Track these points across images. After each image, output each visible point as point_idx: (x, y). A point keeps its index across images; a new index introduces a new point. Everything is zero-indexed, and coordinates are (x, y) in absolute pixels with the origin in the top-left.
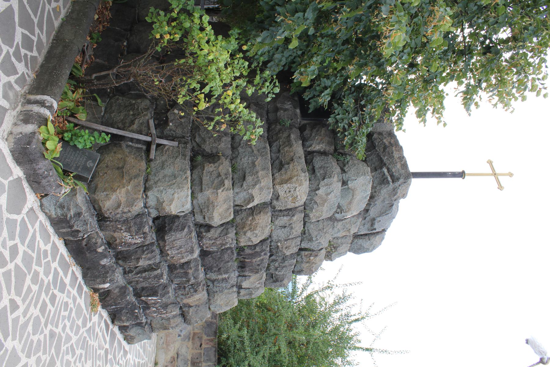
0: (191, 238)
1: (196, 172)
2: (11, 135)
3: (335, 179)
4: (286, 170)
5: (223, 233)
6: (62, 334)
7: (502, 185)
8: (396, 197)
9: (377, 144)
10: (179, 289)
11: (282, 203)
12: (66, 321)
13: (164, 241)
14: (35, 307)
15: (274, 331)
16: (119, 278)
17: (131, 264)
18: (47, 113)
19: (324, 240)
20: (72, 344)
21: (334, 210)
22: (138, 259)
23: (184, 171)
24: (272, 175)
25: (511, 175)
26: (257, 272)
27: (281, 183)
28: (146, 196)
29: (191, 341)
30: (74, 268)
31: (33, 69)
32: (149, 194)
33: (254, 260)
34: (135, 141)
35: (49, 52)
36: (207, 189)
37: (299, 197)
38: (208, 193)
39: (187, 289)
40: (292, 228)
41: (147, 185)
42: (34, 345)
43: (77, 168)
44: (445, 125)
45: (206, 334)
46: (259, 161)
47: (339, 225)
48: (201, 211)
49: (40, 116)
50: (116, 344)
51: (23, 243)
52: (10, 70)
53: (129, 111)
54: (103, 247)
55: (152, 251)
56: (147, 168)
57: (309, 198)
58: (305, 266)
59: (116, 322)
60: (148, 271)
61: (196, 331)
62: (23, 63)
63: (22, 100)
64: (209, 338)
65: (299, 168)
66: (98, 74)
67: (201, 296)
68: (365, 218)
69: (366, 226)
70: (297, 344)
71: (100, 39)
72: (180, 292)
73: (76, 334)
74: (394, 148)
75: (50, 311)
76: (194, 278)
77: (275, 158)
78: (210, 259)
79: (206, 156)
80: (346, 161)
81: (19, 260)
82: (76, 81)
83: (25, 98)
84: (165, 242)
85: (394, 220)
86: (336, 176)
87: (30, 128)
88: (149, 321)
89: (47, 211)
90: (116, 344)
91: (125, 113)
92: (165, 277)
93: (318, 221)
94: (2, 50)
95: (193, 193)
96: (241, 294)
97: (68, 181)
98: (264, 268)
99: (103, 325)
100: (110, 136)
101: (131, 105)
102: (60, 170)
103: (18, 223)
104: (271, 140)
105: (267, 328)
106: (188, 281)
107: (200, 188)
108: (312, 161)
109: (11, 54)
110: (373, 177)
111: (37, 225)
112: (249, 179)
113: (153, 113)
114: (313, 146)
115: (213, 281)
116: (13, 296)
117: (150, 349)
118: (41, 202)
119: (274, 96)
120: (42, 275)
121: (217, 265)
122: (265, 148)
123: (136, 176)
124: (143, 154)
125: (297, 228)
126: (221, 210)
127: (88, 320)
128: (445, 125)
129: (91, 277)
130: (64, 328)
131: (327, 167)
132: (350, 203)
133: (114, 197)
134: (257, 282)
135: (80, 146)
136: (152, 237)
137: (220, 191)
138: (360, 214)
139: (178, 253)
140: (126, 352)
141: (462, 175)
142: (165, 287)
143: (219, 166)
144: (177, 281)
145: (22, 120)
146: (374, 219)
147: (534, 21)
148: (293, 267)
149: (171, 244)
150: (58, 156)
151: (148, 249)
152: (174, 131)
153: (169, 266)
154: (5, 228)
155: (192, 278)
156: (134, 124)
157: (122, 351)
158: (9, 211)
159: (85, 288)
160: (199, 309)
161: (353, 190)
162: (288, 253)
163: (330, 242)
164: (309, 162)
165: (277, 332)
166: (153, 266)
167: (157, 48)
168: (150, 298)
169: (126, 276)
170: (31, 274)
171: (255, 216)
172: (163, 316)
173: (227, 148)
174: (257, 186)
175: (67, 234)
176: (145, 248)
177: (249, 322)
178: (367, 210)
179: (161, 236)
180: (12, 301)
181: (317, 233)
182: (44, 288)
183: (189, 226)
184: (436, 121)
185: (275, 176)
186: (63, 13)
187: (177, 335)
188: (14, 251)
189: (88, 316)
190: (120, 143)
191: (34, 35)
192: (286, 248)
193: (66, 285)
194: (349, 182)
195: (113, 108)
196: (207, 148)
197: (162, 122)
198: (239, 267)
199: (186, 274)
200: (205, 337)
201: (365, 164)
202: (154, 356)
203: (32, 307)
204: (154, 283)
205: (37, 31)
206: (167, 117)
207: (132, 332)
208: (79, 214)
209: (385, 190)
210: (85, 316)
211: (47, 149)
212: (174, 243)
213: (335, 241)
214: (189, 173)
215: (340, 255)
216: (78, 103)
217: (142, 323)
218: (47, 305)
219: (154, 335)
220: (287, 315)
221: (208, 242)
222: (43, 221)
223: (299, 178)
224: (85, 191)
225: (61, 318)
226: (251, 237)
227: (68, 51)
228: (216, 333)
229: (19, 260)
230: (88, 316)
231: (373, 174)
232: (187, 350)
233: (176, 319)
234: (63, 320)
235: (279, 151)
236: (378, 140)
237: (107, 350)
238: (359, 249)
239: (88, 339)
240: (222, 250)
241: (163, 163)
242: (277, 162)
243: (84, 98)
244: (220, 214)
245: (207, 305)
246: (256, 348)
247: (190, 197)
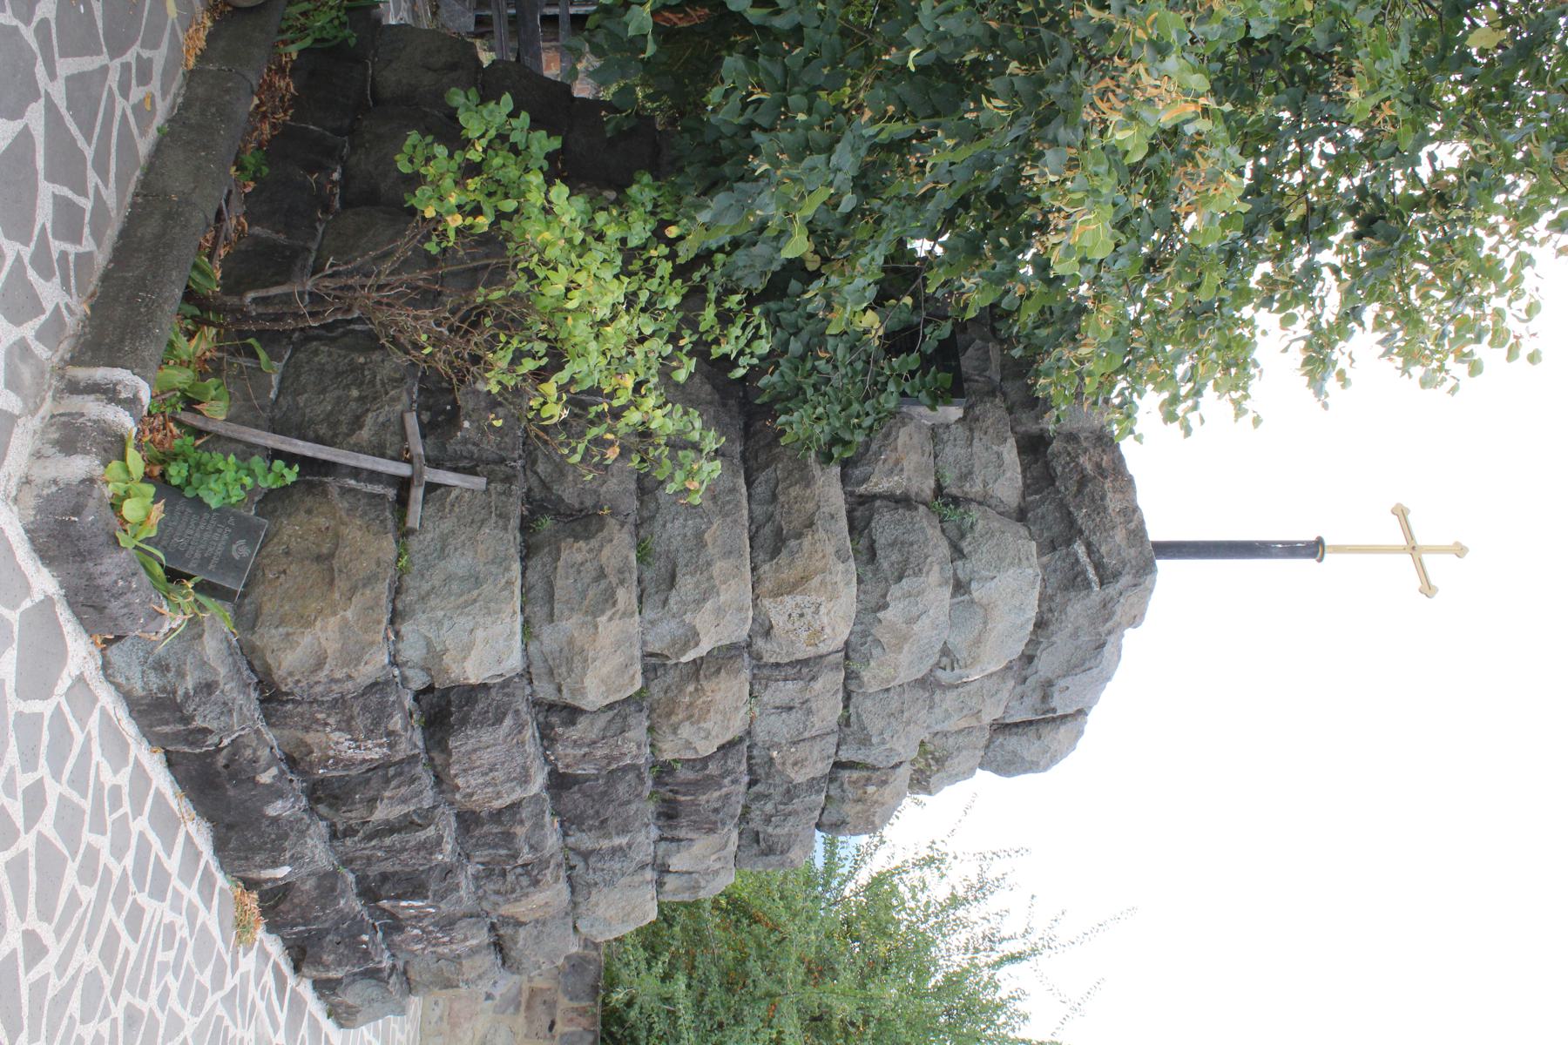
0: (523, 743)
1: (536, 563)
3: (934, 577)
4: (792, 553)
5: (614, 728)
6: (158, 1014)
7: (1433, 582)
8: (1109, 625)
9: (1059, 470)
10: (487, 877)
11: (780, 645)
12: (169, 977)
13: (446, 751)
14: (89, 947)
15: (766, 984)
16: (317, 851)
17: (353, 815)
18: (125, 422)
19: (903, 741)
20: (185, 1039)
22: (372, 802)
23: (501, 562)
24: (753, 569)
25: (1460, 551)
26: (711, 831)
27: (777, 593)
28: (397, 634)
30: (192, 827)
31: (81, 288)
32: (405, 628)
35: (123, 234)
36: (567, 613)
37: (828, 630)
38: (570, 624)
39: (511, 878)
40: (809, 712)
41: (400, 606)
43: (204, 562)
44: (1257, 421)
45: (566, 992)
46: (715, 532)
47: (949, 700)
50: (304, 1030)
52: (21, 304)
53: (348, 387)
54: (274, 771)
55: (413, 780)
56: (400, 555)
57: (859, 628)
58: (850, 810)
59: (305, 970)
60: (399, 831)
61: (539, 983)
62: (57, 280)
63: (54, 383)
64: (575, 1004)
65: (830, 550)
66: (262, 293)
67: (552, 894)
68: (1025, 680)
69: (1028, 701)
70: (835, 1024)
71: (265, 170)
72: (490, 887)
73: (196, 1010)
74: (1108, 484)
75: (127, 952)
76: (531, 847)
78: (577, 796)
80: (968, 521)
81: (46, 824)
82: (199, 306)
83: (63, 377)
84: (450, 755)
86: (936, 568)
87: (79, 466)
88: (400, 965)
89: (121, 680)
90: (304, 1030)
91: (337, 393)
92: (448, 848)
93: (887, 690)
95: (526, 624)
96: (667, 887)
97: (180, 600)
98: (732, 817)
99: (269, 978)
101: (355, 369)
102: (159, 571)
103: (46, 723)
105: (747, 975)
107: (546, 609)
108: (869, 523)
109: (26, 260)
110: (1044, 567)
111: (94, 721)
112: (687, 584)
113: (415, 389)
114: (874, 480)
115: (586, 855)
116: (32, 922)
117: (403, 1039)
118: (104, 657)
119: (755, 361)
120: (105, 857)
121: (597, 812)
122: (733, 490)
123: (370, 580)
124: (388, 513)
125: (825, 711)
126: (605, 670)
127: (49, 230)
128: (1257, 421)
130: (163, 999)
131: (912, 544)
132: (978, 642)
133: (306, 640)
135: (214, 503)
136: (412, 740)
137: (603, 619)
138: (1008, 668)
139: (486, 785)
141: (1314, 549)
142: (448, 871)
143: (602, 546)
144: (481, 855)
145: (56, 443)
146: (1049, 684)
147: (1498, 148)
148: (817, 813)
150: (153, 534)
151: (401, 774)
152: (474, 444)
153: (458, 815)
154: (13, 741)
155: (526, 849)
156: (361, 427)
159: (221, 880)
160: (547, 930)
161: (985, 608)
163: (922, 743)
164: (858, 526)
165: (776, 988)
166: (415, 818)
168: (404, 903)
169: (336, 843)
170: (79, 857)
172: (440, 950)
173: (626, 490)
174: (709, 605)
175: (176, 737)
176: (391, 771)
177: (694, 957)
178: (1028, 659)
180: (30, 937)
182: (112, 890)
183: (517, 712)
184: (1230, 409)
185: (761, 571)
186: (162, 110)
188: (35, 799)
189: (228, 959)
190: (322, 484)
191: (85, 194)
192: (795, 764)
193: (170, 875)
194: (974, 585)
195: (303, 379)
196: (568, 494)
197: (441, 416)
198: (659, 815)
199: (508, 837)
200: (564, 1002)
201: (1023, 532)
204: (416, 862)
205: (93, 178)
206: (454, 402)
207: (349, 997)
208: (208, 687)
209: (1078, 607)
210: (220, 958)
211: (124, 521)
212: (474, 757)
213: (937, 741)
214: (516, 567)
215: (954, 778)
216: (208, 368)
217: (380, 970)
218: (119, 938)
219: (415, 1003)
220: (804, 940)
221: (569, 751)
224: (227, 627)
226: (693, 739)
227: (177, 229)
229: (46, 824)
230: (228, 959)
231: (1045, 559)
234: (161, 977)
236: (1064, 459)
238: (1010, 763)
239: (227, 1021)
240: (612, 772)
241: (444, 541)
242: (767, 530)
244: (602, 679)
245: (570, 920)
247: (518, 637)
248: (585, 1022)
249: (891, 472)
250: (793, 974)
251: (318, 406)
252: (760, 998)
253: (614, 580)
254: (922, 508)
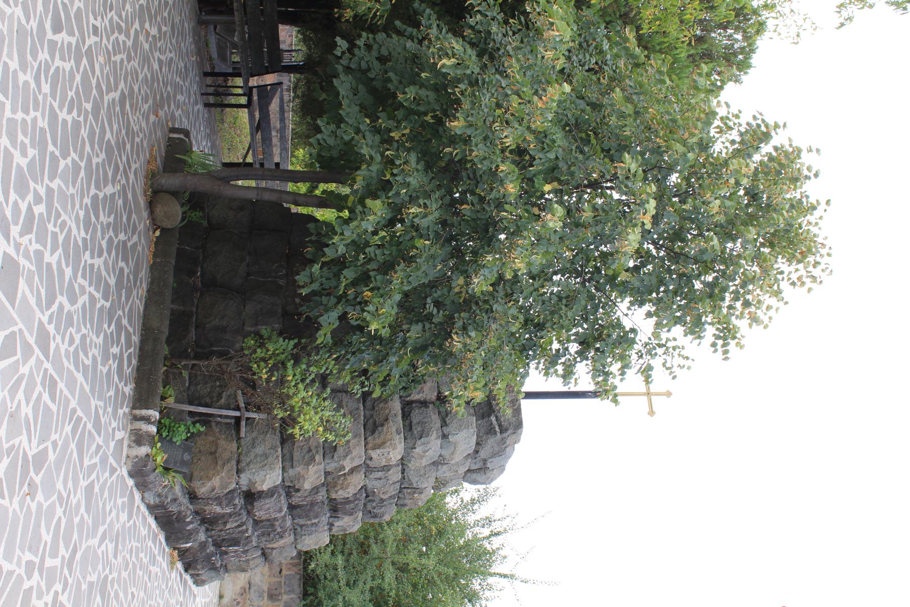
1: (286, 446)
16: (202, 537)
22: (225, 523)
24: (365, 439)
27: (374, 449)
38: (299, 469)
53: (215, 381)
65: (394, 429)
67: (289, 539)
77: (368, 416)
87: (144, 450)
95: (283, 468)
115: (302, 526)
122: (358, 409)
123: (229, 460)
132: (453, 453)
159: (167, 549)
164: (406, 415)
178: (476, 452)
210: (60, 493)
233: (256, 561)
235: (374, 408)
241: (254, 440)
242: (371, 421)
248: (295, 569)
249: (419, 393)
250: (391, 548)
251: (203, 390)
253: (314, 451)
254: (431, 406)
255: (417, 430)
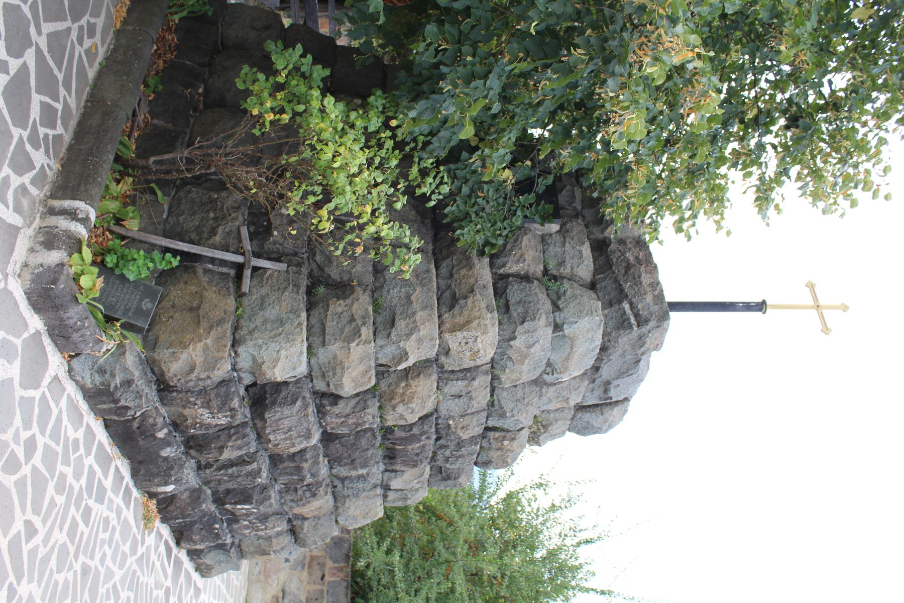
0: (307, 415)
1: (315, 313)
2: (25, 269)
3: (542, 321)
4: (461, 308)
8: (643, 349)
9: (615, 260)
10: (287, 492)
11: (454, 360)
12: (106, 547)
13: (264, 420)
14: (61, 530)
16: (190, 476)
18: (82, 231)
19: (524, 415)
21: (541, 370)
22: (221, 449)
23: (296, 312)
24: (439, 317)
25: (845, 308)
26: (415, 466)
27: (453, 330)
28: (236, 353)
29: (306, 570)
32: (241, 350)
33: (410, 447)
34: (217, 262)
35: (80, 124)
36: (333, 341)
37: (482, 352)
38: (334, 348)
39: (300, 492)
40: (471, 398)
41: (237, 337)
42: (60, 588)
43: (126, 311)
44: (728, 233)
45: (331, 558)
47: (551, 392)
48: (324, 375)
49: (69, 235)
50: (182, 579)
51: (43, 433)
52: (22, 164)
53: (208, 211)
55: (244, 436)
56: (237, 308)
57: (499, 350)
58: (494, 455)
59: (183, 544)
60: (236, 465)
61: (316, 553)
62: (42, 150)
63: (41, 209)
64: (336, 565)
65: (483, 305)
68: (594, 381)
69: (596, 393)
70: (485, 578)
71: (161, 87)
72: (289, 497)
73: (121, 566)
74: (642, 269)
75: (82, 533)
76: (312, 475)
79: (332, 286)
82: (122, 165)
84: (266, 422)
85: (642, 383)
86: (544, 316)
87: (55, 257)
88: (237, 541)
89: (79, 379)
90: (182, 579)
91: (200, 216)
92: (264, 475)
93: (516, 386)
94: (12, 137)
95: (310, 347)
97: (112, 333)
98: (427, 458)
99: (162, 549)
100: (178, 258)
101: (211, 201)
102: (100, 316)
103: (37, 402)
104: (439, 256)
105: (434, 550)
106: (302, 480)
107: (321, 339)
108: (505, 290)
109: (25, 139)
110: (606, 316)
111: (64, 402)
112: (401, 324)
113: (246, 213)
114: (508, 266)
115: (343, 480)
116: (30, 516)
117: (238, 584)
118: (69, 365)
120: (70, 479)
121: (350, 455)
122: (428, 271)
123: (220, 322)
124: (231, 284)
125: (480, 398)
126: (354, 374)
128: (728, 233)
129: (144, 475)
131: (530, 303)
132: (567, 359)
133: (184, 356)
134: (416, 481)
135: (132, 278)
136: (244, 414)
137: (353, 345)
138: (585, 374)
139: (286, 439)
140: (198, 591)
141: (761, 306)
142: (264, 488)
143: (353, 303)
144: (283, 479)
145: (42, 243)
146: (608, 383)
147: (868, 77)
148: (475, 456)
149: (275, 425)
151: (238, 433)
155: (309, 476)
156: (215, 235)
157: (192, 589)
158: (23, 386)
159: (135, 493)
160: (320, 522)
161: (572, 339)
162: (465, 436)
163: (535, 417)
164: (499, 293)
165: (451, 558)
166: (246, 458)
167: (254, 131)
168: (239, 507)
169: (200, 472)
170: (55, 479)
171: (411, 381)
172: (260, 533)
173: (366, 271)
174: (414, 337)
175: (109, 411)
176: (232, 431)
178: (596, 368)
179: (258, 412)
180: (28, 524)
181: (513, 405)
183: (304, 398)
185: (444, 317)
187: (284, 560)
188: (30, 446)
189: (139, 537)
192: (463, 428)
194: (565, 326)
195: (182, 207)
196: (334, 273)
198: (385, 457)
199: (299, 469)
200: (330, 564)
201: (594, 295)
202: (244, 594)
203: (57, 529)
204: (246, 483)
205: (62, 92)
207: (208, 559)
208: (128, 383)
209: (625, 339)
212: (279, 423)
214: (304, 315)
215: (553, 437)
217: (226, 545)
218: (78, 525)
219: (245, 564)
220: (467, 530)
221: (333, 420)
222: (73, 394)
223: (482, 322)
224: (139, 348)
225: (98, 544)
226: (405, 413)
227: (111, 121)
228: (348, 557)
232: (300, 585)
233: (281, 539)
235: (451, 275)
237: (168, 589)
238: (586, 428)
239: (139, 573)
240: (358, 432)
241: (263, 299)
242: (448, 293)
243: (135, 190)
244: (354, 377)
245: (333, 517)
246: (415, 582)
247: (305, 355)
248: (342, 575)
249: (518, 262)
250: (461, 550)
251: (190, 222)
252: (442, 563)
254: (536, 282)
255: (516, 311)
